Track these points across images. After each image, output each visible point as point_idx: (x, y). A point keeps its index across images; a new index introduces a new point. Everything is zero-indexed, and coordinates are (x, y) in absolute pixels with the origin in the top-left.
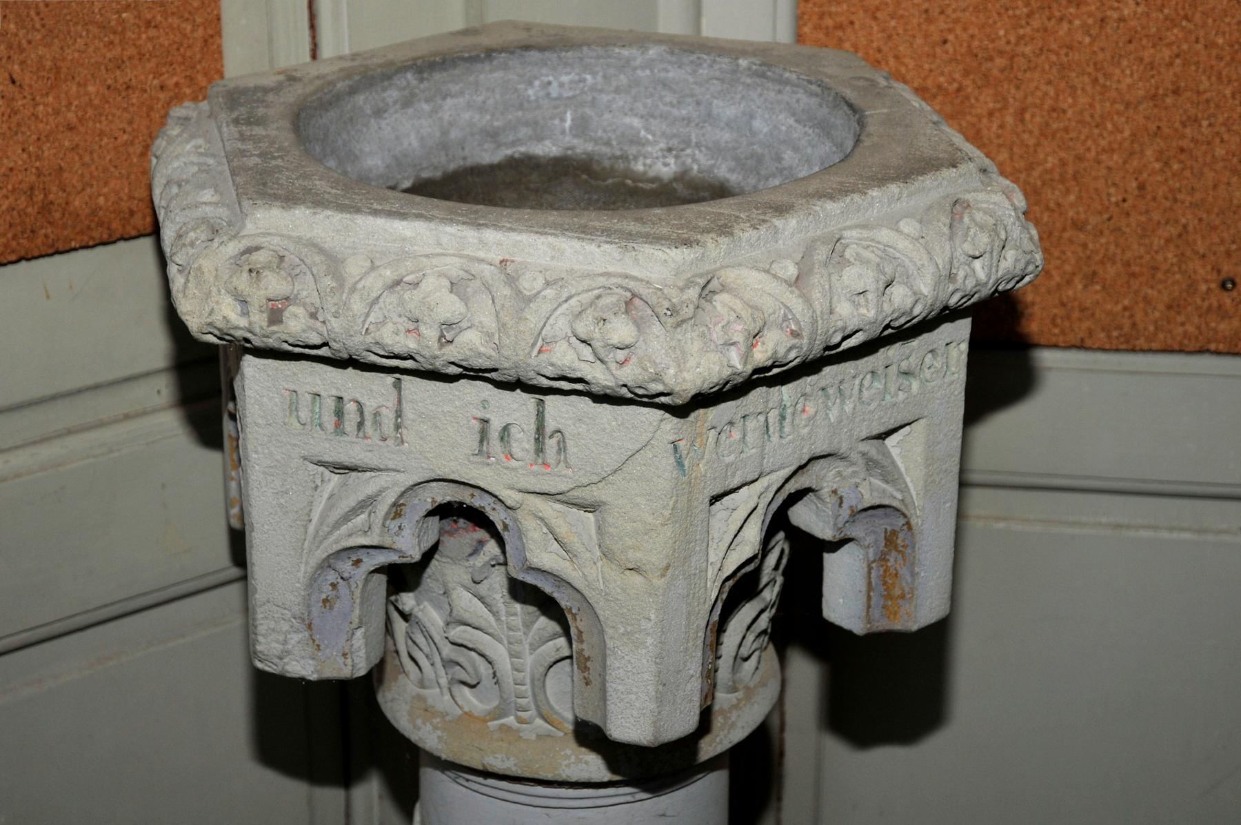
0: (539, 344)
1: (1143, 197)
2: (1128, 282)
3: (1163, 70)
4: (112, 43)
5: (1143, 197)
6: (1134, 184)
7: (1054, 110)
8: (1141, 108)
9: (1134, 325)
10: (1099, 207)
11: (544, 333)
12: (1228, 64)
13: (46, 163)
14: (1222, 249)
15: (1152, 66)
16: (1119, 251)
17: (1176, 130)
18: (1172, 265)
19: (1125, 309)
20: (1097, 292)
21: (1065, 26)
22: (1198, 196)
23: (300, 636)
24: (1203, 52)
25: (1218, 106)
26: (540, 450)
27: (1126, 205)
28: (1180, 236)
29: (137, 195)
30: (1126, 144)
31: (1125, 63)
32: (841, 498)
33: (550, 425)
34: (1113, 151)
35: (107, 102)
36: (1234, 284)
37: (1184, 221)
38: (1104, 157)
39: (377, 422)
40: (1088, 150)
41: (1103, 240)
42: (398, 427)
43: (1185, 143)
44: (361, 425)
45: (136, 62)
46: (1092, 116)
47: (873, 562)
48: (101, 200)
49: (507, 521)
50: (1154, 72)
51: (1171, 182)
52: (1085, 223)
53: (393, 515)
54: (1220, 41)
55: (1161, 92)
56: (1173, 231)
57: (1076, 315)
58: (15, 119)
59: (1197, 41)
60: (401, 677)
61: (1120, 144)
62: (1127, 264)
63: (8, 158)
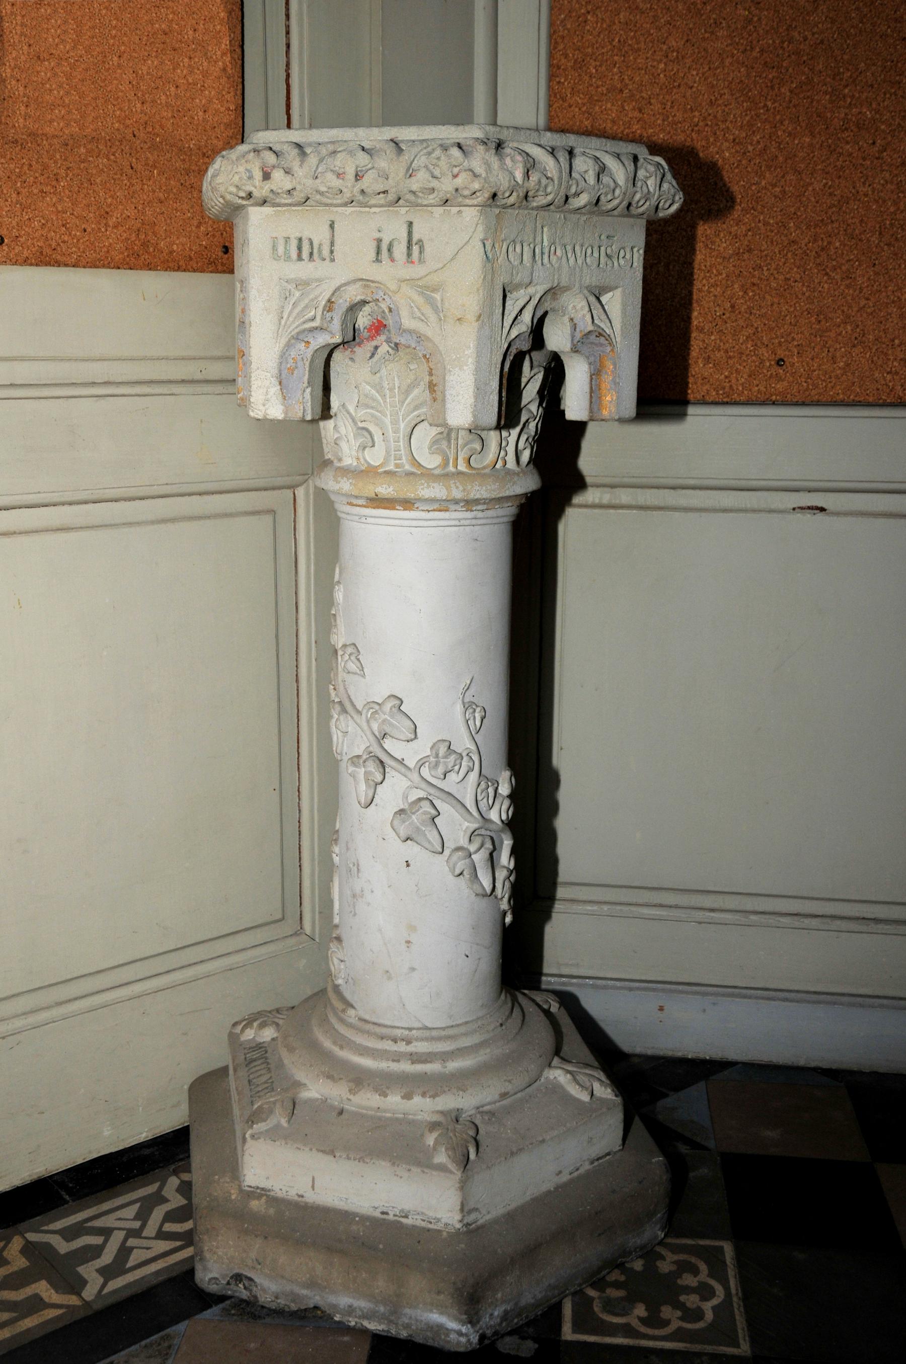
0: (411, 171)
1: (734, 312)
2: (727, 362)
3: (742, 238)
4: (184, 160)
5: (734, 312)
6: (729, 305)
7: (685, 263)
8: (731, 260)
9: (731, 386)
10: (710, 319)
11: (413, 165)
12: (776, 234)
13: (147, 218)
14: (777, 341)
15: (736, 236)
16: (722, 344)
17: (750, 272)
18: (750, 351)
19: (726, 377)
20: (710, 368)
21: (690, 214)
22: (763, 311)
23: (276, 389)
24: (762, 228)
25: (772, 259)
26: (409, 255)
27: (724, 317)
28: (754, 334)
29: (194, 249)
30: (724, 282)
31: (722, 235)
32: (575, 324)
33: (415, 238)
34: (717, 285)
35: (181, 193)
36: (783, 361)
37: (756, 325)
38: (712, 290)
39: (320, 251)
40: (704, 285)
41: (713, 338)
42: (332, 252)
43: (755, 281)
44: (311, 254)
45: (196, 174)
46: (705, 266)
47: (594, 374)
48: (175, 247)
49: (391, 306)
50: (737, 240)
51: (748, 303)
52: (703, 329)
53: (328, 308)
54: (772, 222)
55: (741, 251)
56: (750, 331)
57: (700, 381)
58: (132, 189)
59: (759, 221)
60: (340, 988)
61: (721, 282)
62: (726, 351)
63: (127, 210)
